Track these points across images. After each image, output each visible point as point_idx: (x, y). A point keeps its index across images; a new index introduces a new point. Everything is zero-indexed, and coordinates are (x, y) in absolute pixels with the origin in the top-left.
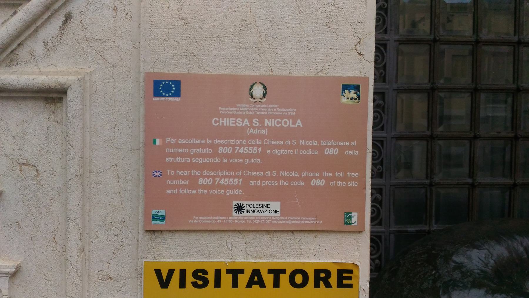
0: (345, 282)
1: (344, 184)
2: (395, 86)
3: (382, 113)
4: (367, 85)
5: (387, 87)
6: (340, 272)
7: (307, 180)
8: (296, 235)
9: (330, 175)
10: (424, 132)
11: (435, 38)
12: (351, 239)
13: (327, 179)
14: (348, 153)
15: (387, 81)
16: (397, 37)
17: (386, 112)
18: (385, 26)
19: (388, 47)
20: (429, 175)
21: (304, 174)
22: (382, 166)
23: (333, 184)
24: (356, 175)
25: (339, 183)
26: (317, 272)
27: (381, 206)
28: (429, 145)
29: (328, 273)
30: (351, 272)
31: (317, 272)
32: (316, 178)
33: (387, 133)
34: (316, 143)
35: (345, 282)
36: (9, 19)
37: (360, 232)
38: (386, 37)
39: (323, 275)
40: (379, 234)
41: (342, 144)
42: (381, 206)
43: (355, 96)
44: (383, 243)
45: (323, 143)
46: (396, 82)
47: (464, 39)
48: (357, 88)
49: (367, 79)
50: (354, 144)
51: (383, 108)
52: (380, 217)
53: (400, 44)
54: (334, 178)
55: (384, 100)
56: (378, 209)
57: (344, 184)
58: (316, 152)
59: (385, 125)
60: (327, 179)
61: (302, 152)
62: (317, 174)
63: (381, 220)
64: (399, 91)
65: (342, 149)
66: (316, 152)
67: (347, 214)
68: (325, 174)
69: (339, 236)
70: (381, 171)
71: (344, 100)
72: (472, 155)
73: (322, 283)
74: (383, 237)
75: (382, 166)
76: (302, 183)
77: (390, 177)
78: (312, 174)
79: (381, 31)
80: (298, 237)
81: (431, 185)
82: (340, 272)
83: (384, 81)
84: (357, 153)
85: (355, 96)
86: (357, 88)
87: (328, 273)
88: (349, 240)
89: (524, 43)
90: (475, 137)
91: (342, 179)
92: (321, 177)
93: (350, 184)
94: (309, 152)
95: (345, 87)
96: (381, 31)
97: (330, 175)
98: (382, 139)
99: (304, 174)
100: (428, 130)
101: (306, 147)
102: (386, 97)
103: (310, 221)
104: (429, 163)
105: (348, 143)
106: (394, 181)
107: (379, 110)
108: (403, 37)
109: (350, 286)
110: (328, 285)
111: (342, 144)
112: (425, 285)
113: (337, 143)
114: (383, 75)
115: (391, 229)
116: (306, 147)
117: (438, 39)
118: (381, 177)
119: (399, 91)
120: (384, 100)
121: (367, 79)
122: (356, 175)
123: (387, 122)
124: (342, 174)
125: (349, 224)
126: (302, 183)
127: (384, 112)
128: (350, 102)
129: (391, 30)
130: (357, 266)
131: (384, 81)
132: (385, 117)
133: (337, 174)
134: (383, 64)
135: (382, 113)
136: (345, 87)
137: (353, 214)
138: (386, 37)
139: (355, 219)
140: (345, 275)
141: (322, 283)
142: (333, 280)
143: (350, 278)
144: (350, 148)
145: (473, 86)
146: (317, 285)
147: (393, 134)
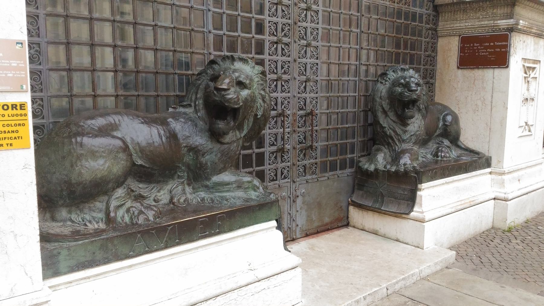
0: (23, 108)
1: (20, 76)
2: (46, 40)
3: (39, 55)
4: (25, 43)
5: (41, 40)
6: (21, 105)
7: (6, 74)
8: (3, 93)
9: (14, 72)
10: (65, 67)
11: (67, 15)
12: (24, 94)
13: (14, 74)
14: (20, 65)
15: (41, 37)
16: (44, 12)
17: (41, 54)
18: (37, 5)
19: (39, 17)
20: (70, 90)
21: (5, 72)
22: (42, 85)
23: (16, 75)
24: (24, 73)
25: (18, 75)
26: (12, 105)
27: (43, 107)
28: (69, 74)
29: (16, 105)
30: (24, 105)
31: (12, 105)
32: (9, 73)
33: (43, 66)
34: (8, 62)
35: (23, 108)
36: (518, 190)
37: (27, 91)
38: (38, 11)
39: (14, 106)
40: (43, 124)
41: (18, 62)
42: (43, 107)
43: (21, 46)
44: (46, 130)
45: (11, 62)
46: (46, 37)
47: (84, 16)
48: (22, 44)
49: (25, 41)
50: (22, 62)
51: (40, 51)
52: (43, 115)
53: (47, 16)
54: (16, 74)
55: (39, 47)
56: (41, 110)
57: (20, 76)
58: (8, 65)
59: (42, 62)
60: (14, 74)
61: (3, 65)
62: (10, 72)
63: (44, 116)
64: (49, 43)
65: (18, 64)
66: (8, 65)
67: (21, 86)
68: (12, 72)
69: (19, 93)
70: (41, 88)
71: (17, 47)
72: (93, 80)
73: (14, 108)
74: (45, 125)
75: (42, 85)
76: (4, 75)
77: (47, 92)
78: (8, 72)
79: (35, 7)
80: (4, 94)
81: (71, 96)
82: (21, 105)
83: (39, 37)
84: (23, 65)
85: (21, 46)
86: (22, 44)
87: (16, 105)
88: (24, 94)
89: (116, 21)
90: (94, 70)
91: (19, 74)
92: (11, 73)
93: (22, 76)
94: (6, 65)
95: (17, 43)
96: (35, 7)
97: (14, 72)
98: (41, 70)
99: (5, 72)
100: (67, 65)
101: (5, 63)
102: (41, 46)
103: (8, 88)
104: (69, 84)
105: (20, 62)
106: (49, 94)
107: (37, 53)
108: (48, 12)
109: (25, 109)
110: (17, 109)
111: (18, 62)
112: (65, 135)
113: (16, 62)
114: (38, 33)
115: (50, 121)
116: (5, 63)
117: (68, 15)
118: (42, 92)
119: (49, 43)
120: (39, 47)
121: (25, 41)
122: (24, 73)
123: (43, 60)
124: (19, 72)
125: (22, 89)
126: (4, 75)
127: (40, 55)
128: (20, 48)
129: (41, 8)
130: (27, 103)
131: (39, 37)
132: (41, 58)
133: (17, 72)
134: (38, 26)
135: (39, 55)
136: (17, 43)
137: (24, 86)
138: (38, 11)
139: (24, 87)
140: (22, 106)
141: (14, 108)
142: (18, 107)
143: (24, 107)
144: (21, 64)
145: (91, 42)
146: (12, 109)
147: (47, 67)
